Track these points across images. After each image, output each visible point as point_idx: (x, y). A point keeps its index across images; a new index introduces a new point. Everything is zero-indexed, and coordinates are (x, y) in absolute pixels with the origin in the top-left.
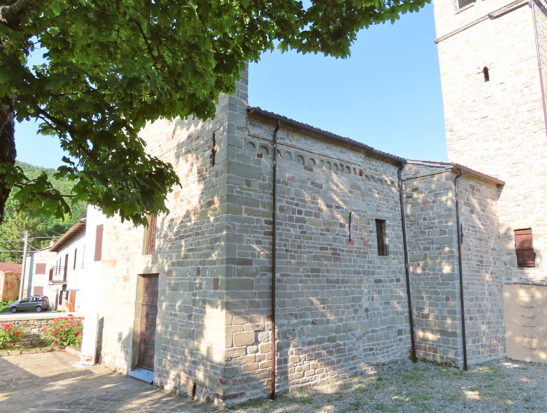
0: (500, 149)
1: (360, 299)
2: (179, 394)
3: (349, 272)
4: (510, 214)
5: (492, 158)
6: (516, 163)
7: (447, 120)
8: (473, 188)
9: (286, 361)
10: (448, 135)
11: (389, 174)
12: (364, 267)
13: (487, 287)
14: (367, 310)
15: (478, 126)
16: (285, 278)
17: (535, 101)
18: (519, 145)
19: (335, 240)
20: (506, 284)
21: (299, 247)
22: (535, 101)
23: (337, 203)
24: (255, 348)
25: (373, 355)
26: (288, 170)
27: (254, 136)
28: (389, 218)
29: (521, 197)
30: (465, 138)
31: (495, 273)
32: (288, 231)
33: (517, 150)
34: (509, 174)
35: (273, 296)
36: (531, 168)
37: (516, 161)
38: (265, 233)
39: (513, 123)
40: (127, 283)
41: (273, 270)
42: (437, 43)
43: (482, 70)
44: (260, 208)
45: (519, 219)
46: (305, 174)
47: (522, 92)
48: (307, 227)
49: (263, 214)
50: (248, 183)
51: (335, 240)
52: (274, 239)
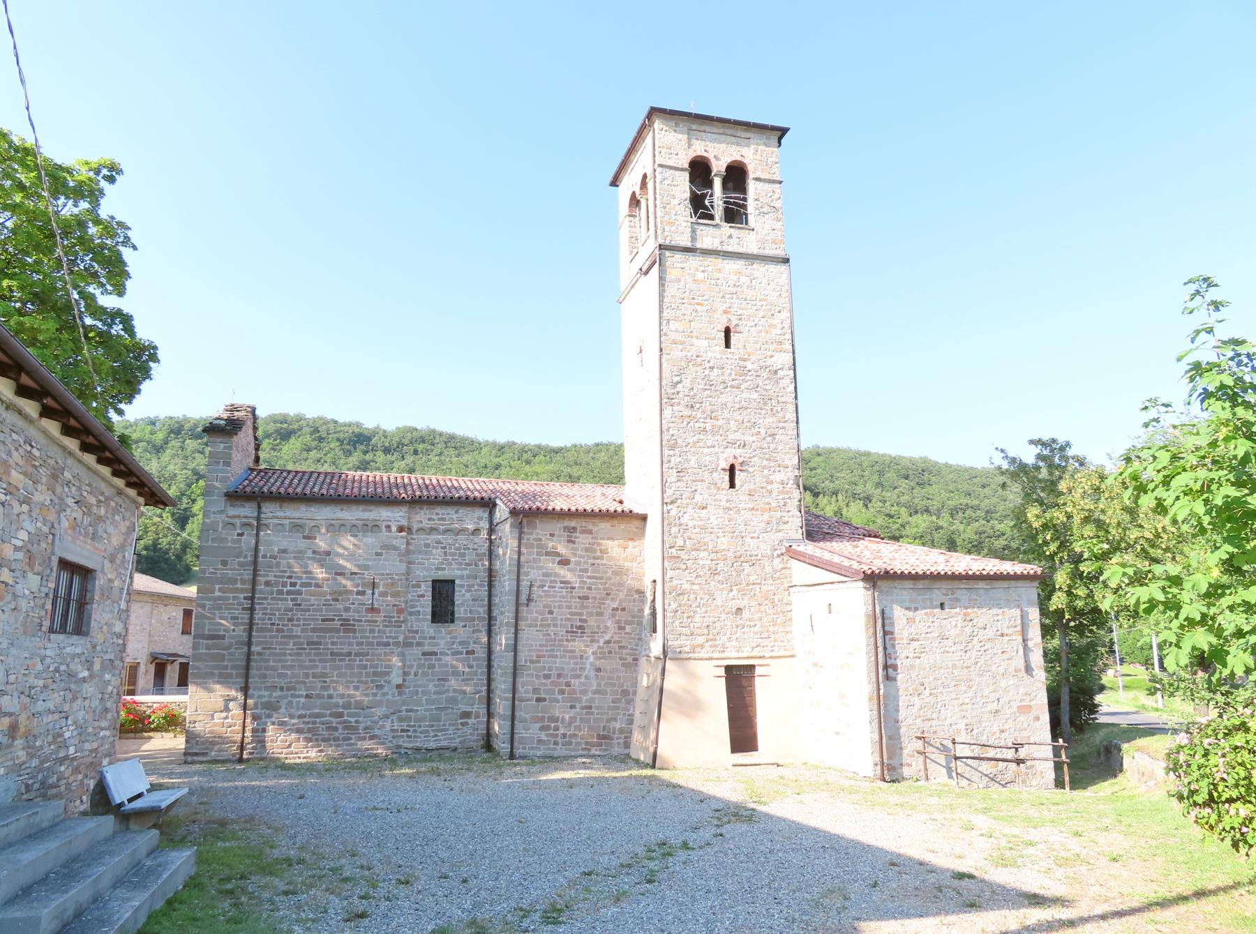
1: (388, 674)
2: (433, 931)
9: (264, 730)
12: (397, 637)
13: (591, 659)
14: (398, 686)
16: (268, 652)
19: (347, 610)
21: (290, 620)
23: (569, 570)
24: (224, 714)
25: (409, 737)
26: (273, 541)
27: (235, 517)
28: (462, 577)
32: (271, 607)
35: (248, 668)
38: (244, 609)
40: (443, 629)
44: (239, 586)
46: (302, 544)
48: (303, 600)
49: (242, 591)
50: (224, 563)
52: (252, 614)
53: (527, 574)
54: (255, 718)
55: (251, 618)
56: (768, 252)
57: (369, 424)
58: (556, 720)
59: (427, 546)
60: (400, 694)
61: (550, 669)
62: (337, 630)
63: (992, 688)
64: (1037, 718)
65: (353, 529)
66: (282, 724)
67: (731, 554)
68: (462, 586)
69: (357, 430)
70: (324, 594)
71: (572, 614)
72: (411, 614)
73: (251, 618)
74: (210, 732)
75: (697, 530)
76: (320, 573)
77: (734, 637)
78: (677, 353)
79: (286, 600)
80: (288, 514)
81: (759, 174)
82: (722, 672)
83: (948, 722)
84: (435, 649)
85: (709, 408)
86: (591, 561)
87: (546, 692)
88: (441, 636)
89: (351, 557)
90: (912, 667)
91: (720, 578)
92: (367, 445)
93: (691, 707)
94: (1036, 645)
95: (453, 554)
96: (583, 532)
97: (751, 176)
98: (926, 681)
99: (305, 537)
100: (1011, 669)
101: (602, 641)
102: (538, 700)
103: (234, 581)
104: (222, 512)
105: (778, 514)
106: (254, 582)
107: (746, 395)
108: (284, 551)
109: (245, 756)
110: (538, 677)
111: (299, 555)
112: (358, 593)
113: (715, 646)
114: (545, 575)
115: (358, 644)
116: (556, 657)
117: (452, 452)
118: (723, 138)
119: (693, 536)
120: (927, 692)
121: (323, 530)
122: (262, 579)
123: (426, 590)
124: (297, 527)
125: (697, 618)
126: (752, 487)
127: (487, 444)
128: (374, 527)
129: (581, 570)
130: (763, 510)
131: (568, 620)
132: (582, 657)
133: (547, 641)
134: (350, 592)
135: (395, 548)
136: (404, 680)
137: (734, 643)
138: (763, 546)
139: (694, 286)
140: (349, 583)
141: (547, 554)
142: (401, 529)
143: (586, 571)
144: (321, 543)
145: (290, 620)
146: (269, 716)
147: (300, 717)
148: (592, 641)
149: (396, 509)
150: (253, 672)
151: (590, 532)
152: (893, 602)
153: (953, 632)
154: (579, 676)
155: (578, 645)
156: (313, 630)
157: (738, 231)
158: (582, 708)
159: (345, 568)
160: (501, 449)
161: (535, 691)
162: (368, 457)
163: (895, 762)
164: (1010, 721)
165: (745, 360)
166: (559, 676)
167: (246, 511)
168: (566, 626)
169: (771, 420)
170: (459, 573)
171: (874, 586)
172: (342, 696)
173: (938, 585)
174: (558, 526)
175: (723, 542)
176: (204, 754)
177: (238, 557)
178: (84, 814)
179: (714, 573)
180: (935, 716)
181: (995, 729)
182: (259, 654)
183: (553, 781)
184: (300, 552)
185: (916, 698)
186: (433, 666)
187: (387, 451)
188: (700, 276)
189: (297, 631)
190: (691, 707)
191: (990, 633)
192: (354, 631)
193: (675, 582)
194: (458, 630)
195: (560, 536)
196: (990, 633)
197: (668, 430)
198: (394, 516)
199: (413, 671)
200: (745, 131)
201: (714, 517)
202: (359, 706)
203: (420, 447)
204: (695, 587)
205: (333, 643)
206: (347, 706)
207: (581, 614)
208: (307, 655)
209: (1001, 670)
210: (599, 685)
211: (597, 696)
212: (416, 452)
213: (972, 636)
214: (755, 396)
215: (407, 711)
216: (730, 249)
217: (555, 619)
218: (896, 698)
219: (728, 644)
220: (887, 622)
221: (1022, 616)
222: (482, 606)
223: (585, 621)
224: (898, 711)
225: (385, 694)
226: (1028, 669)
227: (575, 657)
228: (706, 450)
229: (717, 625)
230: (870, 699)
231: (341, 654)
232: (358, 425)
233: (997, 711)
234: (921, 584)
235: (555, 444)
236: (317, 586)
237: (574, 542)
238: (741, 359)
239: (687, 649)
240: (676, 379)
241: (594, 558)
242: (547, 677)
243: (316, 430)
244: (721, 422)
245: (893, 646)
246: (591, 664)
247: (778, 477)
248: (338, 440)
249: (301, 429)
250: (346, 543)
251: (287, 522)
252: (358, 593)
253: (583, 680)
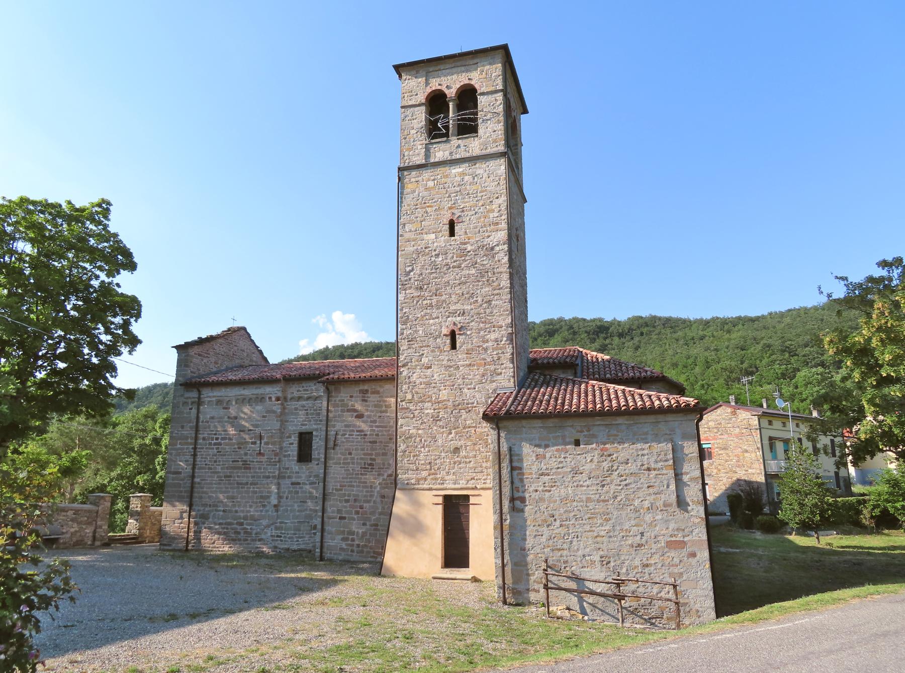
1: (269, 497)
3: (259, 477)
9: (200, 532)
14: (275, 506)
19: (246, 454)
21: (215, 462)
23: (363, 422)
28: (317, 430)
35: (192, 492)
40: (304, 467)
41: (193, 477)
46: (222, 412)
50: (183, 427)
51: (246, 454)
53: (334, 426)
54: (196, 524)
55: (194, 461)
56: (489, 151)
57: (608, 318)
58: (353, 533)
59: (296, 409)
60: (277, 511)
61: (349, 495)
62: (240, 468)
63: (633, 522)
64: (694, 555)
65: (249, 401)
66: (210, 528)
67: (450, 403)
68: (317, 436)
69: (599, 324)
70: (234, 444)
71: (364, 454)
72: (285, 456)
73: (194, 461)
74: (174, 531)
75: (423, 386)
76: (232, 431)
77: (452, 471)
78: (410, 249)
80: (215, 394)
81: (484, 90)
82: (440, 500)
83: (580, 553)
84: (299, 480)
85: (434, 288)
86: (379, 414)
87: (347, 512)
88: (303, 472)
89: (249, 419)
90: (542, 500)
91: (441, 423)
92: (607, 333)
93: (415, 529)
94: (691, 479)
95: (312, 414)
96: (373, 393)
97: (479, 92)
98: (557, 513)
99: (224, 408)
100: (660, 504)
101: (386, 475)
102: (341, 518)
103: (187, 438)
104: (182, 396)
105: (492, 368)
106: (196, 439)
107: (466, 272)
108: (212, 418)
109: (190, 548)
110: (341, 501)
112: (252, 443)
113: (436, 479)
114: (346, 426)
115: (253, 477)
116: (353, 486)
117: (668, 331)
118: (454, 70)
119: (419, 391)
120: (558, 523)
121: (234, 403)
122: (201, 436)
123: (295, 440)
124: (219, 402)
125: (422, 456)
126: (470, 346)
127: (696, 321)
128: (261, 399)
129: (371, 422)
130: (479, 365)
131: (361, 459)
132: (371, 487)
133: (347, 474)
134: (247, 443)
135: (274, 412)
136: (279, 502)
137: (451, 477)
138: (478, 395)
139: (426, 193)
140: (247, 437)
141: (348, 411)
142: (278, 399)
143: (375, 422)
144: (233, 411)
145: (215, 462)
146: (204, 523)
147: (220, 524)
148: (379, 475)
149: (275, 386)
150: (195, 495)
151: (378, 393)
152: (522, 440)
153: (588, 467)
154: (368, 502)
155: (370, 478)
156: (227, 468)
157: (464, 141)
158: (371, 525)
159: (245, 426)
160: (706, 323)
161: (339, 511)
162: (608, 341)
163: (521, 587)
164: (656, 556)
165: (465, 244)
166: (355, 500)
167: (194, 394)
168: (361, 463)
169: (487, 289)
170: (315, 427)
171: (498, 428)
172: (243, 511)
173: (570, 422)
174: (355, 390)
175: (444, 394)
176: (170, 545)
179: (436, 419)
180: (565, 546)
181: (637, 562)
182: (199, 483)
183: (286, 578)
184: (221, 418)
185: (545, 528)
186: (297, 492)
187: (621, 335)
188: (431, 184)
189: (219, 469)
190: (415, 529)
191: (632, 467)
192: (250, 468)
193: (404, 428)
194: (313, 465)
195: (357, 397)
196: (632, 467)
197: (402, 310)
198: (272, 391)
199: (285, 495)
200: (473, 58)
201: (437, 374)
202: (253, 518)
203: (645, 330)
204: (420, 432)
205: (238, 476)
206: (245, 518)
207: (371, 454)
208: (225, 484)
209: (646, 504)
210: (383, 508)
211: (382, 516)
212: (642, 334)
213: (611, 470)
214: (473, 271)
215: (281, 523)
216: (458, 156)
217: (353, 459)
218: (524, 528)
219: (446, 478)
220: (515, 458)
221: (674, 450)
223: (374, 460)
224: (525, 540)
225: (267, 511)
226: (681, 503)
227: (366, 487)
228: (431, 321)
229: (438, 461)
230: (495, 528)
231: (241, 484)
232: (601, 320)
233: (640, 545)
234: (550, 423)
235: (753, 314)
236: (230, 439)
237: (366, 401)
238: (462, 243)
239: (413, 481)
240: (408, 269)
241: (381, 412)
242: (347, 501)
243: (571, 327)
244: (443, 298)
245: (522, 480)
246: (378, 492)
247: (493, 336)
248: (586, 332)
249: (561, 328)
250: (246, 410)
251: (214, 399)
252: (252, 443)
253: (372, 504)
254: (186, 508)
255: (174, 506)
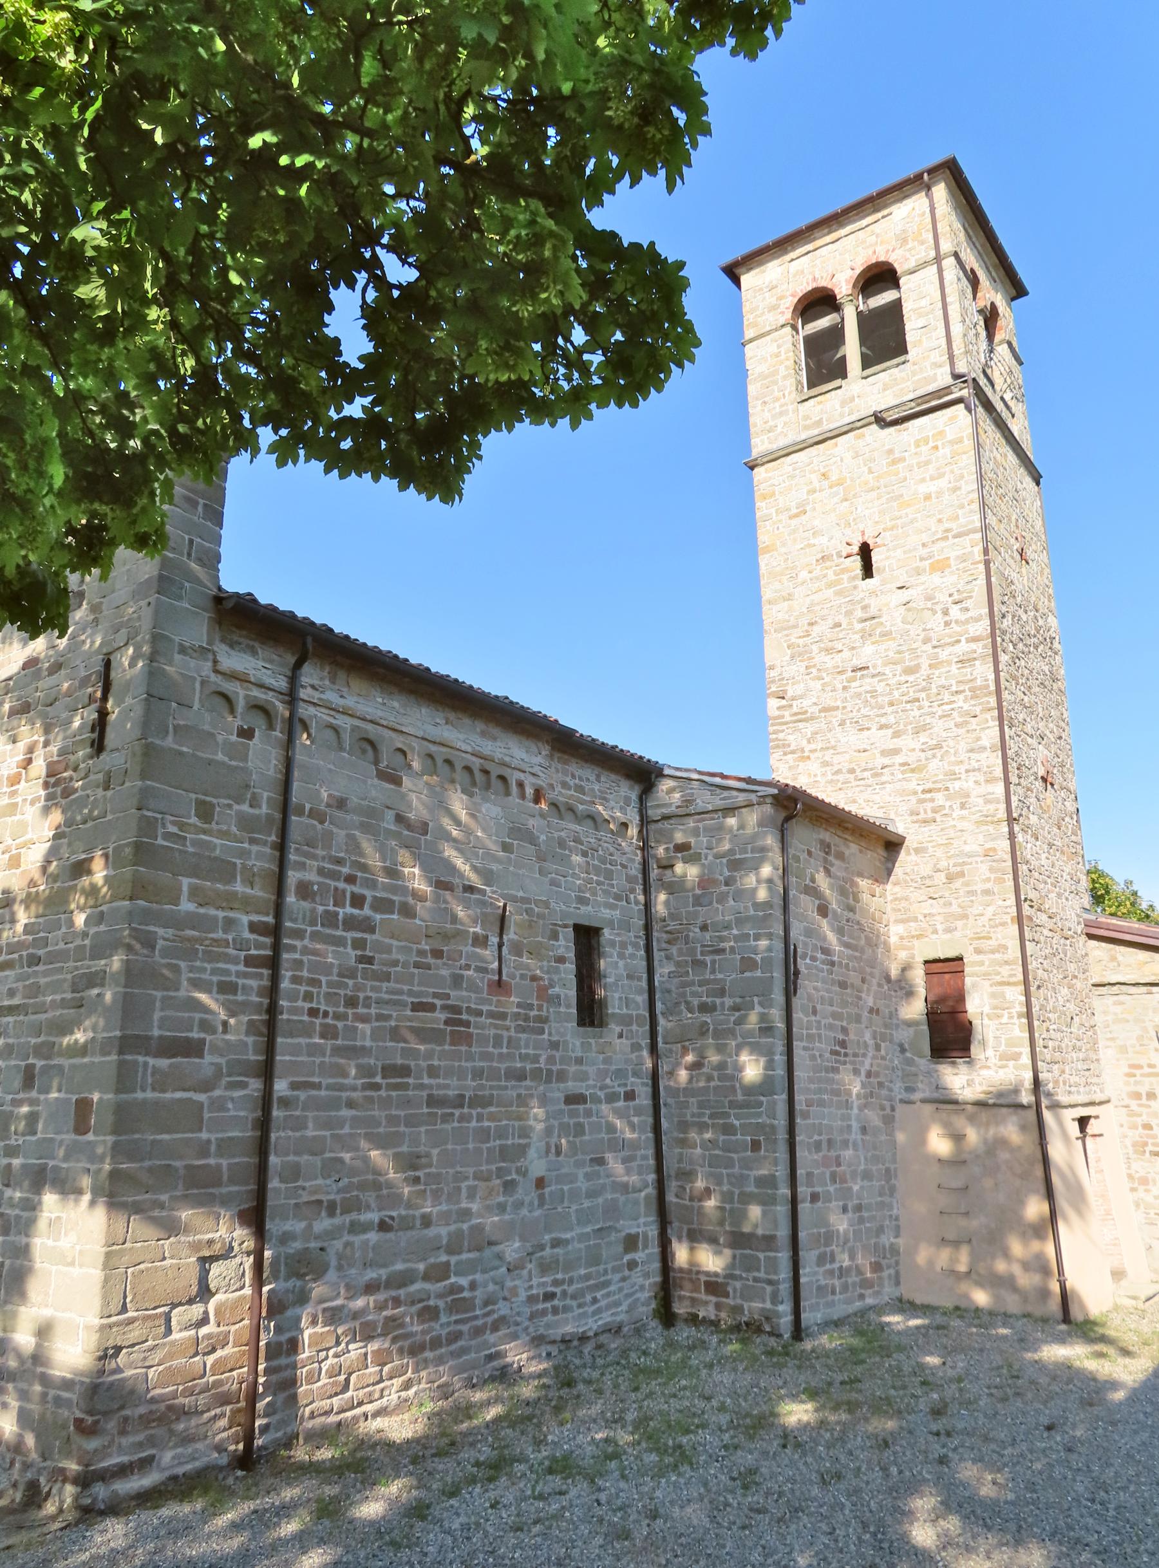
0: (896, 752)
1: (523, 1150)
3: (494, 1074)
4: (916, 919)
5: (876, 775)
6: (930, 791)
7: (772, 668)
8: (826, 848)
9: (293, 1346)
10: (773, 704)
11: (616, 802)
15: (845, 688)
16: (302, 1095)
17: (975, 639)
18: (939, 746)
20: (901, 1101)
21: (352, 1002)
22: (975, 639)
24: (197, 1310)
26: (327, 775)
28: (611, 923)
29: (941, 877)
30: (812, 718)
31: (877, 1075)
33: (934, 756)
34: (915, 818)
36: (963, 806)
37: (929, 786)
38: (250, 961)
39: (923, 690)
42: (752, 468)
43: (856, 549)
44: (239, 887)
45: (935, 932)
46: (378, 790)
47: (946, 612)
49: (247, 904)
50: (205, 812)
51: (457, 981)
66: (333, 1316)
79: (340, 942)
80: (350, 702)
99: (383, 776)
103: (226, 871)
108: (341, 803)
111: (370, 820)
122: (293, 877)
131: (831, 1027)
134: (460, 934)
145: (352, 1002)
146: (302, 1298)
159: (453, 869)
176: (146, 1464)
177: (239, 800)
178: (104, 577)
192: (468, 1039)
222: (640, 993)
254: (229, 1231)
255: (172, 1228)
